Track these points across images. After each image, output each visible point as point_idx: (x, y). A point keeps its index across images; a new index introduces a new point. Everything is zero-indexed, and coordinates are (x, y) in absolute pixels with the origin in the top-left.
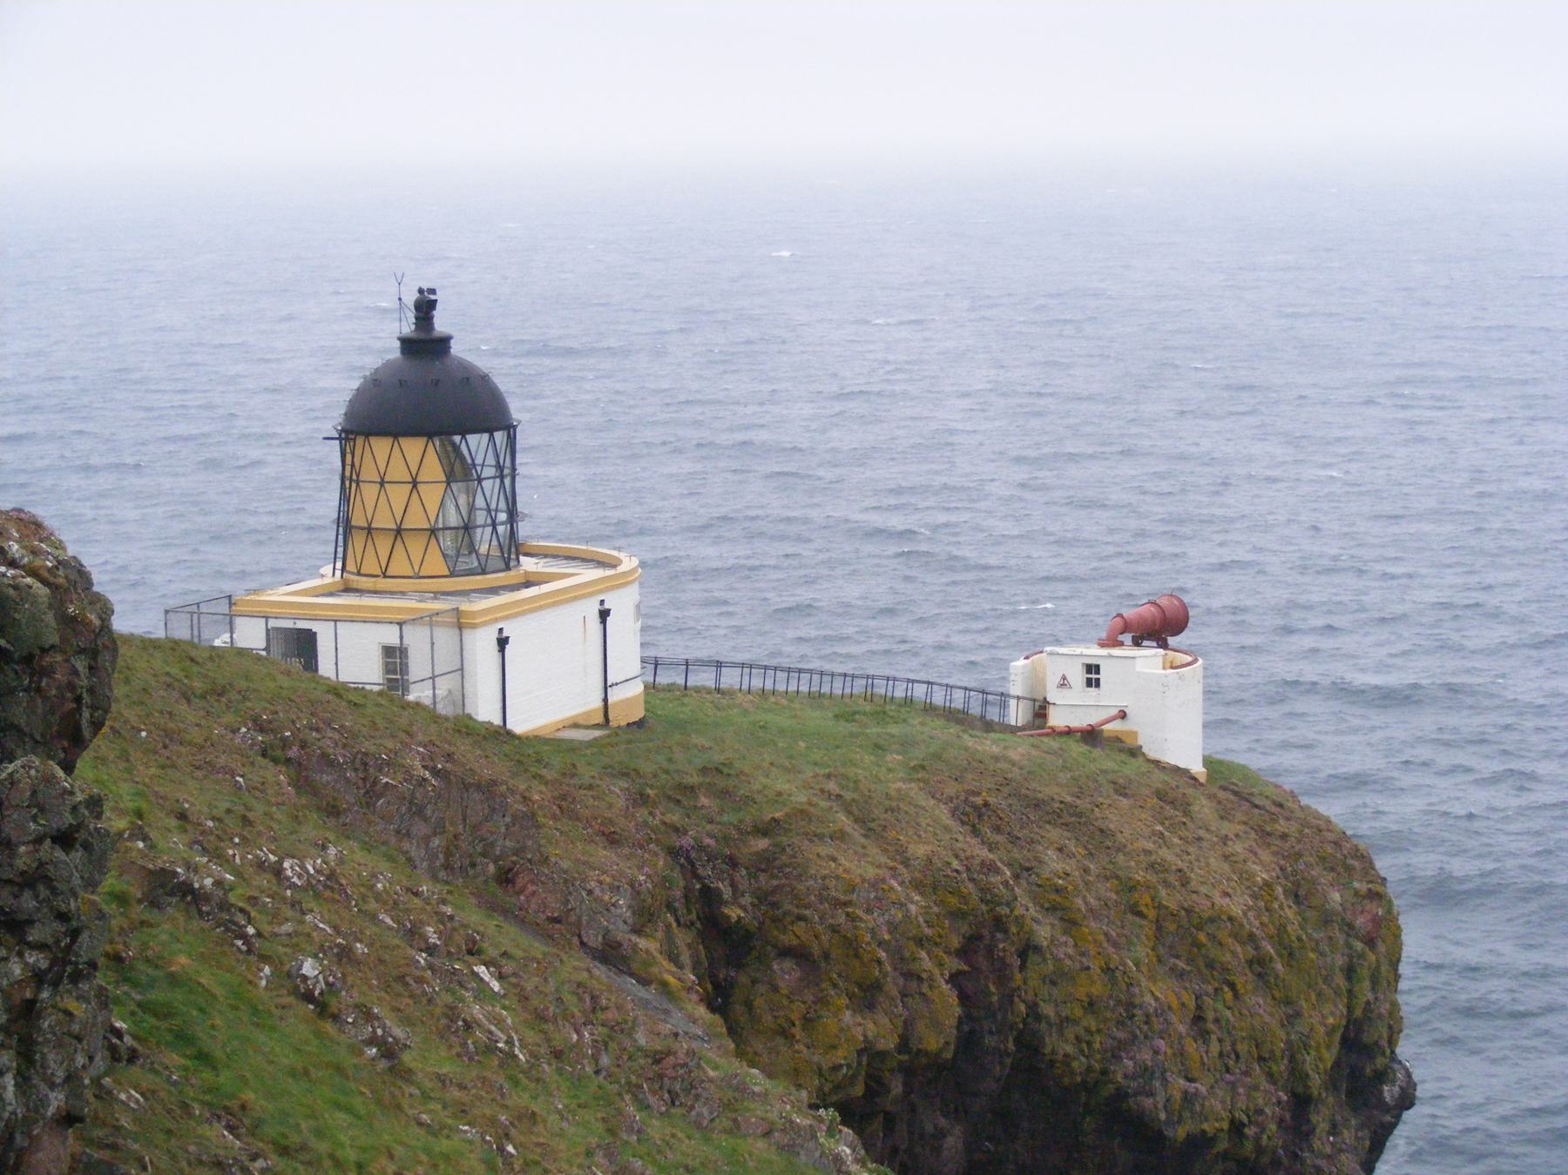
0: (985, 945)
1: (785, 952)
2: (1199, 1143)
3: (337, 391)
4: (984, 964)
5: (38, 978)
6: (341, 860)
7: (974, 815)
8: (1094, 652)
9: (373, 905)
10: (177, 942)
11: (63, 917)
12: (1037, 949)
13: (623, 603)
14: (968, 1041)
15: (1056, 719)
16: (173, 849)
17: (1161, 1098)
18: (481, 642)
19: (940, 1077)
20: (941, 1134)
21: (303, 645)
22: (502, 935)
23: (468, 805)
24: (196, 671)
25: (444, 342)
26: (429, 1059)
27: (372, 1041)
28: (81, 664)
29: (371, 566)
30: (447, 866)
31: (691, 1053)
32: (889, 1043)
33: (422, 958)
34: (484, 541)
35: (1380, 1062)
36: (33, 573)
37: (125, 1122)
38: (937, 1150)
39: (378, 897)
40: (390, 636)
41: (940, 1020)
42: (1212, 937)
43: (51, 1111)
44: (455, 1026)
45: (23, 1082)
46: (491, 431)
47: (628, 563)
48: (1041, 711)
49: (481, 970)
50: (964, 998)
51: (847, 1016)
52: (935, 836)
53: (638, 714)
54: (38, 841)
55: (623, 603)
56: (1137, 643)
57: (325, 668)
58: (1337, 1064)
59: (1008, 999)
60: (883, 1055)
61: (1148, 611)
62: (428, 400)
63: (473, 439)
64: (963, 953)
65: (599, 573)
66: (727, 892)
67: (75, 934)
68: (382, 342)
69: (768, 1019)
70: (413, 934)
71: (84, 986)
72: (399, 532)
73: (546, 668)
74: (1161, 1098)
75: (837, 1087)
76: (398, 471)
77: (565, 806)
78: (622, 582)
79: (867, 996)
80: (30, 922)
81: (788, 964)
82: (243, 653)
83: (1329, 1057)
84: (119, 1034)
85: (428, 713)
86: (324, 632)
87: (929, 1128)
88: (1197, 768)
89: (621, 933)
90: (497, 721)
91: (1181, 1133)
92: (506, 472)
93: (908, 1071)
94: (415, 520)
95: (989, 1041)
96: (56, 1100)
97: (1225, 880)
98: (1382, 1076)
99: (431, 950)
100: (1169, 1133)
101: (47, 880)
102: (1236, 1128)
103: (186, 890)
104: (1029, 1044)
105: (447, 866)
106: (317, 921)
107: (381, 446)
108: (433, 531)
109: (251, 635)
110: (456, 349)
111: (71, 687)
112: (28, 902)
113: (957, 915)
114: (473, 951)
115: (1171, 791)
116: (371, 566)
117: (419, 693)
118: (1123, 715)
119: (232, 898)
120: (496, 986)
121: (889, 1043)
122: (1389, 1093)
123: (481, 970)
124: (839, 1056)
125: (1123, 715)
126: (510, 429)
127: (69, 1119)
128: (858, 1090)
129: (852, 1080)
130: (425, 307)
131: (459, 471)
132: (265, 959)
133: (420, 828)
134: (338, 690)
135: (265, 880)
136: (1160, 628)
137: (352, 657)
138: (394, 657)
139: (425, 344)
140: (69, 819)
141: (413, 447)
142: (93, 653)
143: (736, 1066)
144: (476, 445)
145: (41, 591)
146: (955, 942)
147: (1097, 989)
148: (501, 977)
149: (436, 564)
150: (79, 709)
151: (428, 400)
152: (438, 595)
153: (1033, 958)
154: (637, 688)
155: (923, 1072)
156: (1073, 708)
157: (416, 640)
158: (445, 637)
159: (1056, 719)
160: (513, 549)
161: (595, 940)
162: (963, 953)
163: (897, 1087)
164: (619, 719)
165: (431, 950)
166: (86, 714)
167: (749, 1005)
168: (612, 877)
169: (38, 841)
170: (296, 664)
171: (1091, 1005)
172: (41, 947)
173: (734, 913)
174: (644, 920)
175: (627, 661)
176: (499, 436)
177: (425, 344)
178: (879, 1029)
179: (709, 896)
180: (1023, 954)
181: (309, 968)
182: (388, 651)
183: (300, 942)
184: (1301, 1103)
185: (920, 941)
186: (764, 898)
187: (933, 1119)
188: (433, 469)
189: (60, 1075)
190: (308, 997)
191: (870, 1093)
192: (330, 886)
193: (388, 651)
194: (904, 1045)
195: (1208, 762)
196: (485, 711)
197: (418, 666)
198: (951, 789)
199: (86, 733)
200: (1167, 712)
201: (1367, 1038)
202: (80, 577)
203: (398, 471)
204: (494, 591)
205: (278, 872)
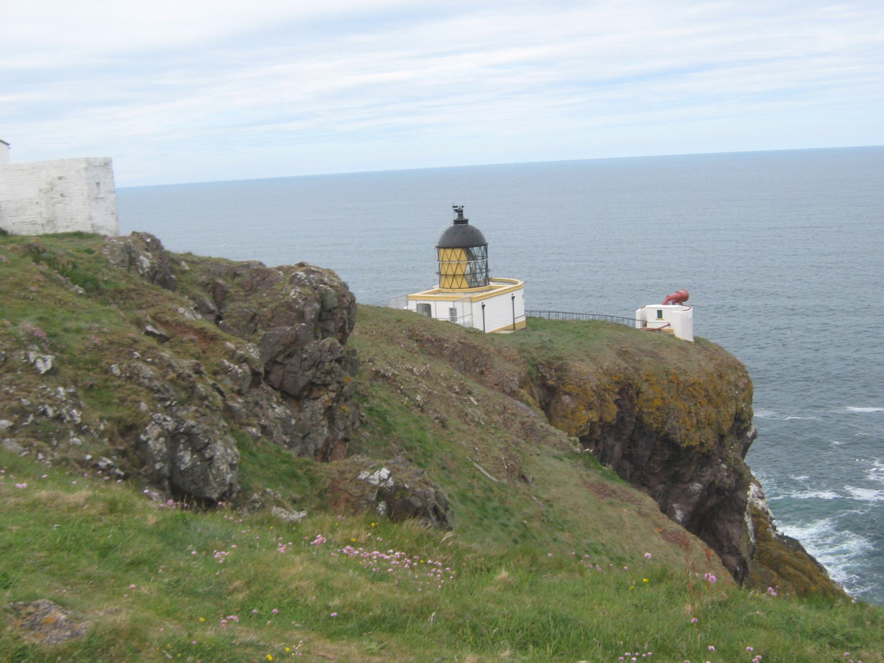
0: (627, 391)
1: (566, 393)
2: (690, 448)
3: (437, 236)
4: (626, 397)
5: (333, 400)
6: (430, 368)
7: (623, 354)
8: (660, 306)
9: (440, 380)
10: (381, 391)
11: (339, 383)
12: (642, 393)
13: (518, 294)
14: (621, 419)
15: (649, 326)
16: (380, 365)
17: (679, 435)
18: (477, 306)
19: (615, 429)
20: (613, 446)
21: (428, 308)
22: (479, 389)
23: (468, 352)
24: (382, 313)
25: (466, 221)
26: (454, 422)
27: (437, 418)
28: (345, 312)
29: (447, 286)
30: (465, 370)
31: (533, 422)
32: (596, 419)
33: (454, 395)
34: (480, 278)
35: (746, 425)
36: (331, 287)
37: (364, 440)
38: (612, 450)
39: (441, 377)
40: (451, 305)
41: (612, 412)
42: (694, 389)
43: (340, 438)
44: (463, 415)
45: (331, 429)
46: (480, 246)
47: (520, 283)
48: (645, 324)
49: (472, 398)
50: (619, 406)
51: (584, 412)
52: (609, 359)
53: (524, 326)
54: (331, 361)
55: (518, 294)
56: (674, 304)
57: (433, 316)
58: (733, 425)
59: (633, 407)
60: (595, 423)
61: (677, 295)
62: (463, 238)
63: (475, 249)
64: (619, 393)
65: (512, 286)
66: (549, 377)
67: (342, 387)
68: (448, 221)
69: (561, 413)
70: (450, 388)
71: (349, 403)
72: (454, 275)
73: (495, 313)
74: (679, 435)
75: (581, 432)
76: (454, 259)
77: (499, 352)
78: (519, 288)
79: (590, 407)
80: (330, 384)
81: (567, 397)
82: (410, 312)
83: (730, 424)
84: (363, 416)
85: (461, 327)
86: (432, 303)
87: (610, 444)
88: (691, 340)
89: (515, 388)
90: (481, 329)
91: (685, 445)
92: (485, 257)
93: (602, 428)
94: (459, 272)
95: (627, 419)
96: (341, 435)
97: (697, 369)
98: (747, 429)
99: (457, 393)
100: (681, 445)
101: (334, 372)
102: (702, 444)
103: (384, 376)
104: (639, 419)
105: (465, 370)
106: (424, 385)
107: (449, 251)
108: (464, 275)
109: (412, 306)
110: (470, 223)
111: (342, 318)
112: (329, 378)
113: (617, 383)
114: (470, 393)
115: (683, 346)
116: (447, 286)
117: (459, 321)
118: (669, 325)
119: (397, 378)
120: (476, 403)
121: (596, 419)
122: (749, 434)
123: (472, 398)
124: (581, 423)
125: (669, 325)
126: (486, 245)
127: (346, 440)
128: (587, 433)
129: (584, 430)
130: (460, 212)
131: (471, 257)
132: (405, 395)
133: (457, 359)
134: (436, 321)
135: (408, 374)
136: (680, 299)
137: (440, 311)
138: (453, 311)
139: (461, 222)
140: (339, 355)
141: (458, 252)
142: (349, 309)
143: (547, 426)
144: (476, 250)
145: (333, 291)
146: (617, 390)
147: (659, 404)
148: (477, 401)
149: (465, 284)
150: (345, 325)
151: (463, 238)
152: (466, 293)
153: (641, 395)
154: (524, 319)
155: (606, 427)
156: (653, 323)
157: (458, 306)
158: (467, 305)
159: (649, 326)
160: (487, 280)
161: (508, 391)
162: (619, 393)
163: (599, 432)
164: (518, 327)
165: (457, 393)
166: (347, 326)
167: (555, 409)
168: (511, 371)
169: (331, 361)
170: (425, 314)
171: (658, 409)
172: (333, 391)
173: (550, 382)
174: (523, 384)
175: (520, 311)
176: (482, 247)
177: (461, 222)
178: (593, 416)
179: (543, 378)
180: (638, 394)
181: (418, 398)
182: (451, 310)
183: (415, 391)
184: (722, 437)
185: (605, 390)
186: (560, 378)
187: (610, 441)
188: (464, 257)
189: (342, 428)
190: (418, 406)
191: (591, 434)
192: (427, 375)
193: (451, 310)
194: (601, 419)
195: (695, 338)
196: (478, 326)
197: (459, 314)
198: (616, 347)
199: (347, 331)
200: (679, 321)
201: (742, 418)
202: (345, 286)
203: (454, 259)
204: (482, 292)
205: (411, 371)
